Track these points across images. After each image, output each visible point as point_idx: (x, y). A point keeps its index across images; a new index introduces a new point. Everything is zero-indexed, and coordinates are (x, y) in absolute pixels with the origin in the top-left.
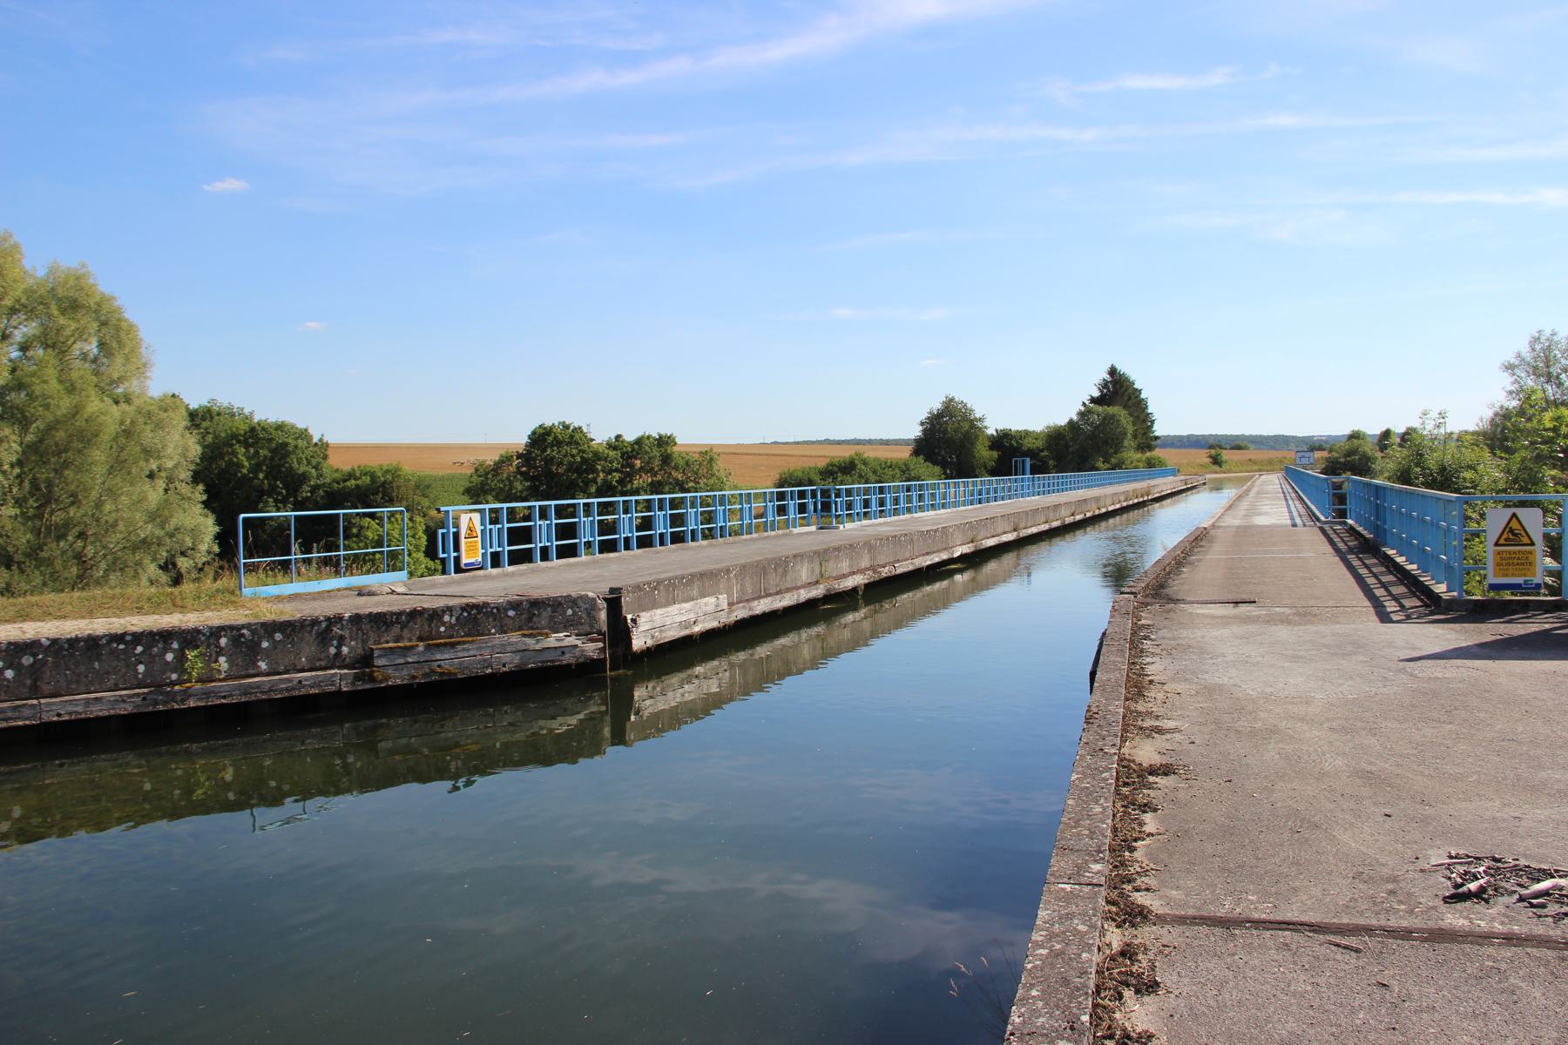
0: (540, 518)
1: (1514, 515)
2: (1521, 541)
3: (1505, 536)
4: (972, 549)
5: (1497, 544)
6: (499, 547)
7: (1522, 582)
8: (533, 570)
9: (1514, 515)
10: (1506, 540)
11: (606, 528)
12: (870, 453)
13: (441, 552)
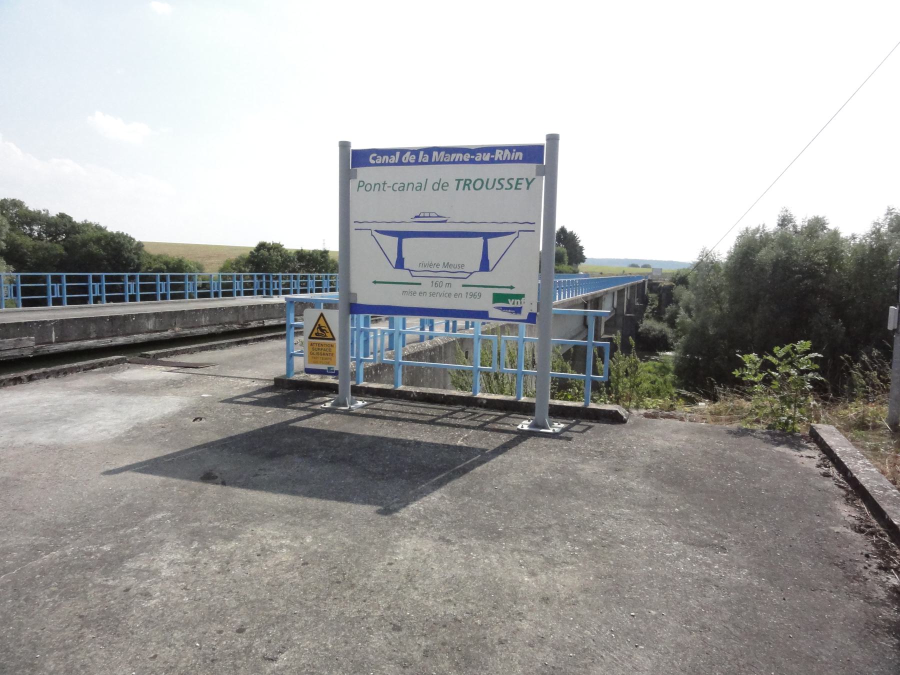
1: (322, 315)
2: (326, 336)
3: (316, 331)
5: (310, 338)
7: (327, 369)
9: (322, 315)
10: (316, 334)
13: (92, 293)
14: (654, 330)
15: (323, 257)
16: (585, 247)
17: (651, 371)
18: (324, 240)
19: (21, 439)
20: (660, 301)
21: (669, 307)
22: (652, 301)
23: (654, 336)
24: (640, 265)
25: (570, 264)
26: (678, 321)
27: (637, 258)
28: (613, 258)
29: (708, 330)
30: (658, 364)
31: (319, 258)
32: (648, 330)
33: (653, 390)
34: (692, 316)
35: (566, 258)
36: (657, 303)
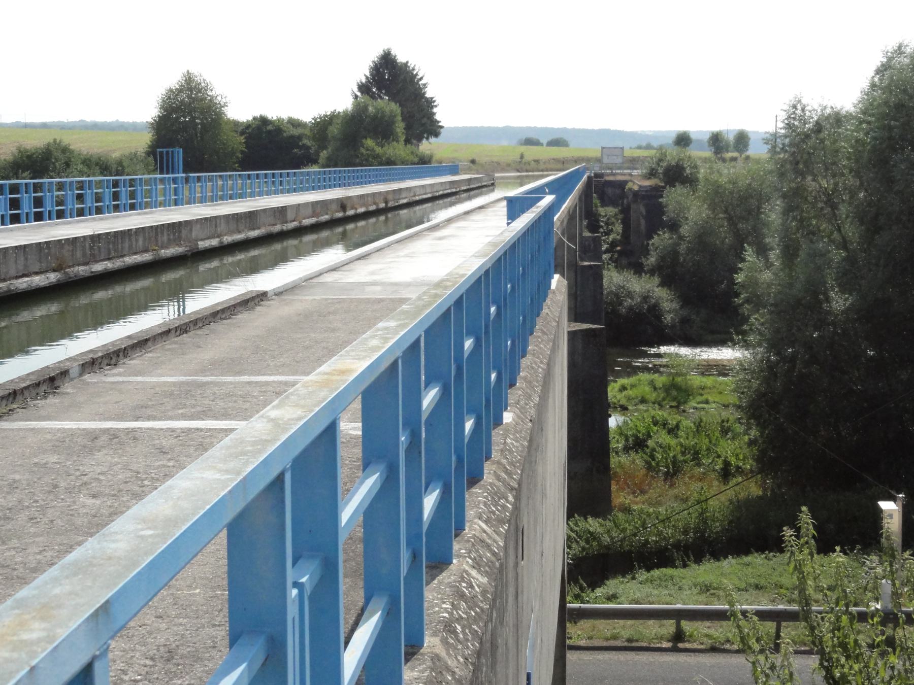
12: (82, 145)
14: (630, 295)
16: (438, 100)
17: (648, 397)
20: (626, 223)
21: (656, 237)
22: (607, 224)
23: (631, 308)
24: (544, 141)
25: (407, 141)
26: (740, 278)
28: (479, 125)
29: (828, 300)
30: (661, 380)
32: (617, 295)
33: (683, 453)
34: (772, 265)
36: (619, 228)
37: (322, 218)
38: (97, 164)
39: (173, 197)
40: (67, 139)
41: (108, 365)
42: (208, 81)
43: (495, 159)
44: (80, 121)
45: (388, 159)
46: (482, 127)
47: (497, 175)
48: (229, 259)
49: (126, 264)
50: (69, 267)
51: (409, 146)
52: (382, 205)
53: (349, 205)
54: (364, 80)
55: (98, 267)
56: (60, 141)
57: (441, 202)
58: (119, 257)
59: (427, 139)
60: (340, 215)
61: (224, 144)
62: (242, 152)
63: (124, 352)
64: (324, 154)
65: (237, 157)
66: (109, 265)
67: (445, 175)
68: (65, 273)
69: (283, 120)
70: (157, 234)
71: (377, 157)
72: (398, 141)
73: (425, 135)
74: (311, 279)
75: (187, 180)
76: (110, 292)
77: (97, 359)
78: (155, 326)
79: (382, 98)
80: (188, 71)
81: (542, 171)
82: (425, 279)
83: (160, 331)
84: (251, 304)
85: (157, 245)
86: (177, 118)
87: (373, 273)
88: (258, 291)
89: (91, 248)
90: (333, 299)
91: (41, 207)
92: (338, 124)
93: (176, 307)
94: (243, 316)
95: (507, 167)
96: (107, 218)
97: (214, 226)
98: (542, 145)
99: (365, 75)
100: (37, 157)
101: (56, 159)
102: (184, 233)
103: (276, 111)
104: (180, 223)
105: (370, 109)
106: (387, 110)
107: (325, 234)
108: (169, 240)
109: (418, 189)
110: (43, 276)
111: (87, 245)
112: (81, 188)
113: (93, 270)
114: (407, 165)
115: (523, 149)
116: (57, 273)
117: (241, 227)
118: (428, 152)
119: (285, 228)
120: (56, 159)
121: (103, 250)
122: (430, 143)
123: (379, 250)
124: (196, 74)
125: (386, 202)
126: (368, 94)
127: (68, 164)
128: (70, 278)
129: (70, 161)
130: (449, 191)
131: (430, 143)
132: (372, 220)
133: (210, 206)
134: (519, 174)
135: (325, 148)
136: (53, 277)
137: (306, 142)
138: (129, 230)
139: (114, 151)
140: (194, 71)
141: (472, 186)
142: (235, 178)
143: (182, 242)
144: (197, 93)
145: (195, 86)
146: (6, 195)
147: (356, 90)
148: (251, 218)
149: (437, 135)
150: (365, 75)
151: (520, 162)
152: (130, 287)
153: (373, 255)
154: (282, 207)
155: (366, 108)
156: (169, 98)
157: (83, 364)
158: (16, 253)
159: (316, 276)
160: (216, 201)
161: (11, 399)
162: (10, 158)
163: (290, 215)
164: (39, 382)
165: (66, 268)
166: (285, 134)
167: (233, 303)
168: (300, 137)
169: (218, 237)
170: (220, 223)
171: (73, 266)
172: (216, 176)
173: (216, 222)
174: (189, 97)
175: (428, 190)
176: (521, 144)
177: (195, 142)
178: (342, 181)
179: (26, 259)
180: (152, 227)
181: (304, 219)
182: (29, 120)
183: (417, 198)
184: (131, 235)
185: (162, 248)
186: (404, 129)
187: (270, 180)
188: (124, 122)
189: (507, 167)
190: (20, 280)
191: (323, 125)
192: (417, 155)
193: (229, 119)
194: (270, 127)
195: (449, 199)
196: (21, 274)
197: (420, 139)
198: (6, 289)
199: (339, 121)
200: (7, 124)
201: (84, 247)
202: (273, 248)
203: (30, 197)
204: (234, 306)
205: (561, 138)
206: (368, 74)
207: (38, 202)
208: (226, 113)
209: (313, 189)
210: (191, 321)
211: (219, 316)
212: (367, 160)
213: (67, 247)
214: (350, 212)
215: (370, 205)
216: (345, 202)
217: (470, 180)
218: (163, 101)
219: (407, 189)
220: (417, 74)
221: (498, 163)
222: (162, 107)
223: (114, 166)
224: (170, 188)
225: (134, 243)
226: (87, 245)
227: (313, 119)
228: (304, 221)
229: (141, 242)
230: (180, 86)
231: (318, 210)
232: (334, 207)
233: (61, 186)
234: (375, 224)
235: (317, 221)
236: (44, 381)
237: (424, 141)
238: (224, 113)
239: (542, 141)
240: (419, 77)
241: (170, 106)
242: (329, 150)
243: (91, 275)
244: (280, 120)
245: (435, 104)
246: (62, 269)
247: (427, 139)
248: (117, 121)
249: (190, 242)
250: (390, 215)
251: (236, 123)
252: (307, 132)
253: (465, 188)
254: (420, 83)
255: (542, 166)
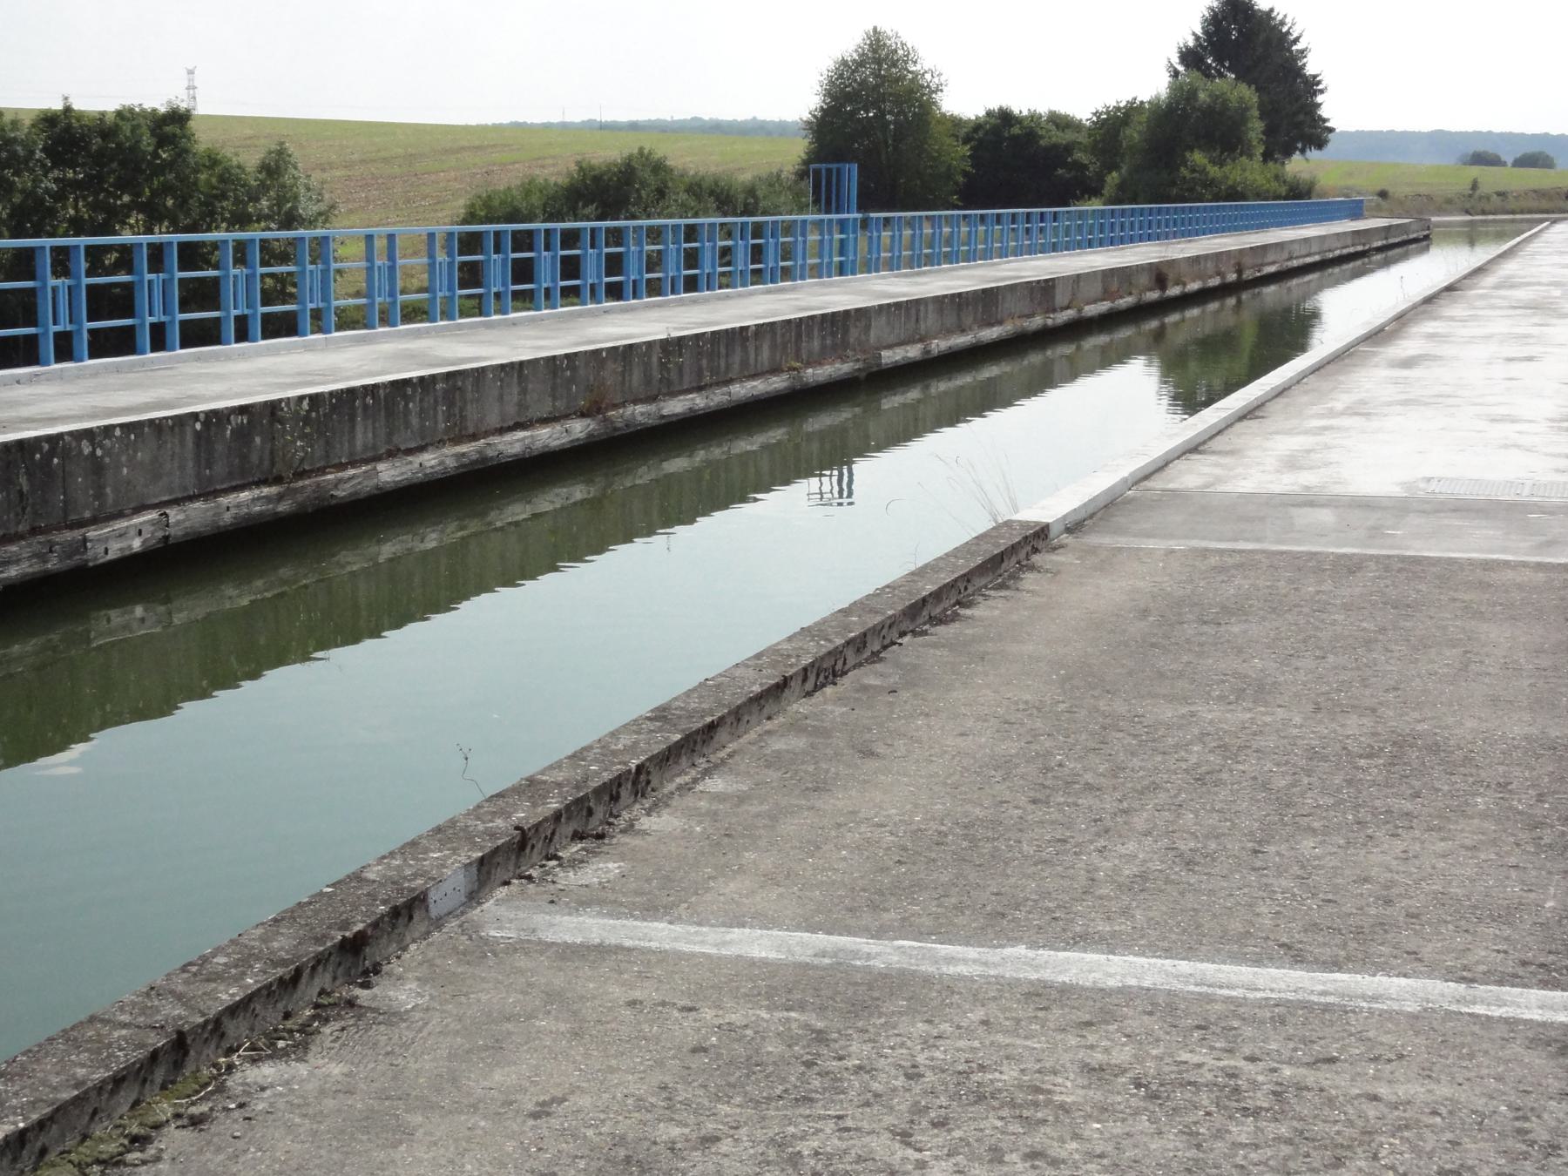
0: (56, 274)
4: (152, 536)
6: (71, 322)
8: (143, 364)
11: (106, 302)
12: (685, 160)
13: (51, 321)
15: (163, 141)
16: (1326, 80)
18: (191, 72)
19: (724, 952)
25: (1267, 156)
27: (1484, 128)
31: (147, 142)
35: (1255, 128)
37: (1121, 301)
38: (712, 193)
39: (836, 259)
40: (662, 149)
41: (578, 836)
42: (909, 46)
43: (1423, 190)
44: (692, 119)
45: (1233, 187)
46: (1391, 132)
47: (1434, 219)
48: (941, 386)
49: (734, 398)
50: (615, 406)
51: (1271, 164)
52: (1232, 277)
53: (1171, 276)
54: (1191, 44)
55: (676, 406)
56: (650, 153)
57: (1336, 270)
58: (719, 384)
59: (1303, 151)
60: (1153, 295)
61: (934, 159)
62: (965, 174)
63: (635, 783)
64: (1113, 178)
65: (956, 183)
66: (699, 401)
67: (1340, 218)
68: (606, 419)
69: (1040, 116)
70: (799, 336)
71: (1210, 183)
72: (1250, 156)
73: (1300, 145)
74: (1147, 477)
75: (865, 224)
76: (701, 455)
77: (537, 827)
78: (743, 665)
79: (1221, 75)
80: (875, 29)
81: (1513, 212)
82: (1433, 486)
83: (757, 689)
84: (1010, 565)
85: (798, 358)
86: (854, 113)
87: (1292, 463)
88: (1024, 525)
89: (663, 366)
90: (1221, 552)
91: (531, 281)
92: (1140, 123)
93: (835, 479)
94: (989, 610)
95: (1447, 205)
96: (706, 300)
97: (913, 319)
98: (1504, 164)
99: (1194, 34)
100: (610, 180)
101: (641, 183)
102: (854, 334)
103: (1028, 100)
104: (847, 312)
105: (1202, 96)
106: (1233, 97)
107: (1125, 333)
108: (823, 347)
109: (1296, 246)
110: (558, 427)
111: (655, 359)
112: (729, 235)
113: (665, 412)
114: (1266, 199)
115: (1475, 171)
116: (588, 421)
117: (968, 320)
118: (1305, 176)
119: (1050, 322)
120: (641, 183)
121: (687, 370)
122: (1307, 160)
123: (1281, 392)
124: (890, 33)
125: (1240, 272)
126: (1199, 69)
127: (661, 193)
128: (616, 429)
129: (666, 187)
130: (1352, 250)
131: (1307, 160)
132: (1213, 306)
133: (906, 275)
134: (1469, 218)
135: (1115, 167)
136: (579, 429)
137: (1079, 156)
138: (742, 328)
139: (740, 169)
140: (886, 27)
141: (1392, 241)
142: (949, 221)
143: (849, 353)
144: (890, 67)
145: (887, 55)
146: (507, 254)
147: (1175, 60)
148: (986, 302)
149: (1320, 144)
150: (1194, 34)
151: (1470, 196)
152: (748, 445)
153: (1271, 407)
154: (1046, 281)
155: (1192, 94)
156: (841, 76)
157: (482, 861)
158: (501, 380)
159: (1160, 469)
160: (919, 266)
161: (159, 1075)
162: (563, 180)
163: (1061, 298)
164: (298, 973)
165: (607, 409)
166: (1042, 143)
167: (964, 565)
168: (1069, 148)
169: (921, 340)
170: (926, 317)
171: (623, 405)
172: (920, 217)
173: (918, 311)
174: (877, 75)
175: (1315, 249)
176: (1465, 164)
177: (883, 157)
178: (1117, 233)
179: (524, 392)
180: (789, 321)
181: (1088, 304)
182: (607, 117)
183: (1295, 263)
184: (747, 339)
185: (808, 364)
186: (1264, 133)
187: (1021, 226)
188: (764, 121)
189: (1447, 205)
190: (508, 437)
191: (1114, 124)
192: (1285, 182)
193: (944, 115)
194: (1016, 130)
195: (1351, 265)
196: (511, 423)
197: (1288, 153)
198: (475, 457)
199: (1144, 118)
200: (573, 123)
201: (647, 366)
202: (1026, 362)
203: (504, 261)
204: (967, 578)
205: (1540, 153)
206: (1199, 32)
207: (614, 264)
208: (940, 103)
209: (1090, 246)
210: (848, 643)
211: (925, 613)
212: (1191, 190)
213: (611, 365)
214: (1174, 291)
215: (1210, 277)
216: (1165, 270)
217: (1388, 229)
218: (830, 82)
219: (1277, 244)
220: (1288, 33)
221: (1430, 198)
222: (828, 93)
223: (741, 197)
224: (831, 241)
225: (752, 356)
226: (655, 359)
227: (1095, 114)
228: (1087, 308)
229: (766, 353)
230: (860, 56)
231: (1114, 286)
232: (1144, 280)
233: (655, 234)
234: (1217, 312)
235: (1111, 309)
236: (320, 961)
237: (1297, 156)
238: (935, 103)
239: (1503, 158)
240: (1292, 38)
241: (842, 90)
242: (1124, 170)
243: (657, 422)
244: (1034, 117)
245: (1320, 87)
246: (599, 411)
247: (1303, 151)
248: (754, 118)
249: (864, 352)
250: (1245, 296)
251: (956, 122)
252: (1082, 138)
253: (1379, 244)
254: (1294, 48)
255: (1512, 205)
